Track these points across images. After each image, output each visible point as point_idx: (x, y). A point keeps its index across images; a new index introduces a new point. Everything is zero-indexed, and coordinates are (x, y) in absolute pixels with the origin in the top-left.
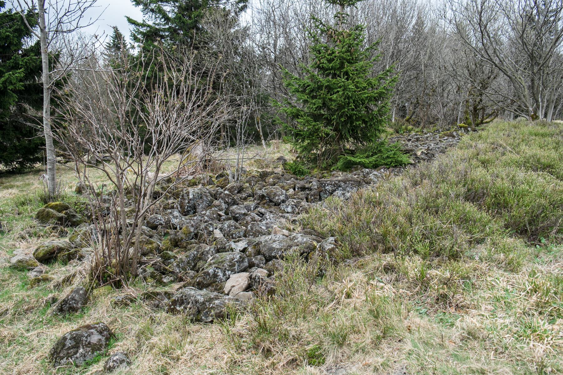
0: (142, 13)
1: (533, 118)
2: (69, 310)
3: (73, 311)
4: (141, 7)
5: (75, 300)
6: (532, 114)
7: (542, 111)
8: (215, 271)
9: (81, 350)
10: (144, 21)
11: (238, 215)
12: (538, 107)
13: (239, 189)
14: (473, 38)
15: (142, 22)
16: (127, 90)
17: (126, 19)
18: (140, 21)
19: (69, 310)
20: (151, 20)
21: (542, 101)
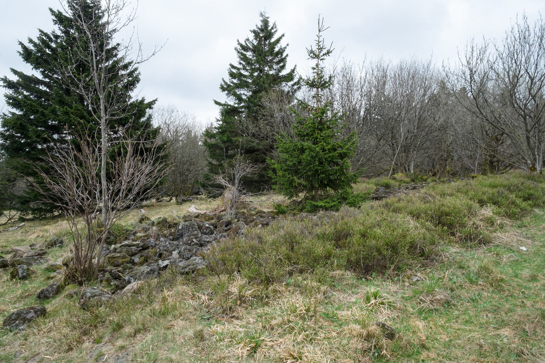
0: (226, 96)
1: (531, 170)
2: (44, 298)
3: (46, 298)
4: (226, 92)
5: (48, 291)
6: (531, 166)
7: (539, 163)
8: (129, 279)
9: (17, 322)
10: (226, 102)
11: (203, 242)
12: (535, 159)
13: (226, 223)
14: (242, 92)
15: (224, 103)
16: (92, 155)
17: (214, 101)
18: (223, 102)
19: (44, 298)
20: (232, 101)
21: (539, 155)
